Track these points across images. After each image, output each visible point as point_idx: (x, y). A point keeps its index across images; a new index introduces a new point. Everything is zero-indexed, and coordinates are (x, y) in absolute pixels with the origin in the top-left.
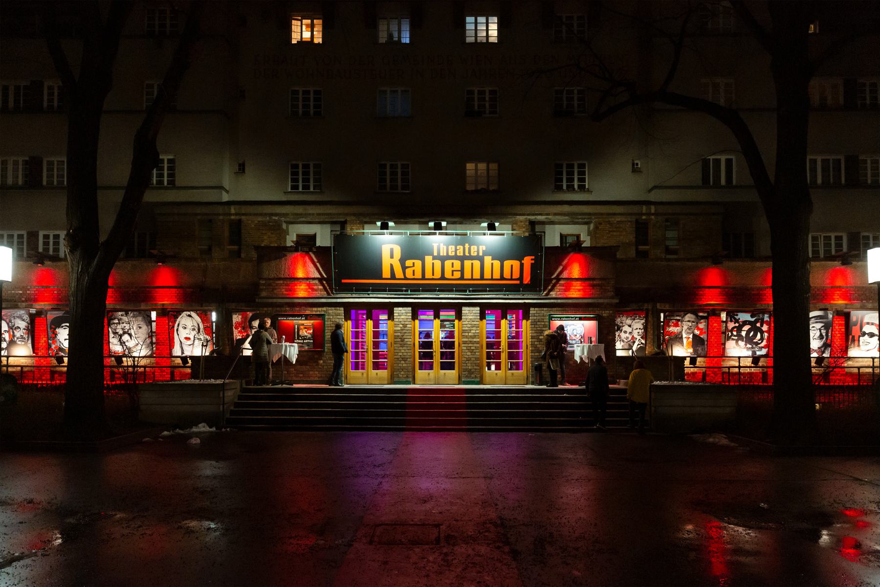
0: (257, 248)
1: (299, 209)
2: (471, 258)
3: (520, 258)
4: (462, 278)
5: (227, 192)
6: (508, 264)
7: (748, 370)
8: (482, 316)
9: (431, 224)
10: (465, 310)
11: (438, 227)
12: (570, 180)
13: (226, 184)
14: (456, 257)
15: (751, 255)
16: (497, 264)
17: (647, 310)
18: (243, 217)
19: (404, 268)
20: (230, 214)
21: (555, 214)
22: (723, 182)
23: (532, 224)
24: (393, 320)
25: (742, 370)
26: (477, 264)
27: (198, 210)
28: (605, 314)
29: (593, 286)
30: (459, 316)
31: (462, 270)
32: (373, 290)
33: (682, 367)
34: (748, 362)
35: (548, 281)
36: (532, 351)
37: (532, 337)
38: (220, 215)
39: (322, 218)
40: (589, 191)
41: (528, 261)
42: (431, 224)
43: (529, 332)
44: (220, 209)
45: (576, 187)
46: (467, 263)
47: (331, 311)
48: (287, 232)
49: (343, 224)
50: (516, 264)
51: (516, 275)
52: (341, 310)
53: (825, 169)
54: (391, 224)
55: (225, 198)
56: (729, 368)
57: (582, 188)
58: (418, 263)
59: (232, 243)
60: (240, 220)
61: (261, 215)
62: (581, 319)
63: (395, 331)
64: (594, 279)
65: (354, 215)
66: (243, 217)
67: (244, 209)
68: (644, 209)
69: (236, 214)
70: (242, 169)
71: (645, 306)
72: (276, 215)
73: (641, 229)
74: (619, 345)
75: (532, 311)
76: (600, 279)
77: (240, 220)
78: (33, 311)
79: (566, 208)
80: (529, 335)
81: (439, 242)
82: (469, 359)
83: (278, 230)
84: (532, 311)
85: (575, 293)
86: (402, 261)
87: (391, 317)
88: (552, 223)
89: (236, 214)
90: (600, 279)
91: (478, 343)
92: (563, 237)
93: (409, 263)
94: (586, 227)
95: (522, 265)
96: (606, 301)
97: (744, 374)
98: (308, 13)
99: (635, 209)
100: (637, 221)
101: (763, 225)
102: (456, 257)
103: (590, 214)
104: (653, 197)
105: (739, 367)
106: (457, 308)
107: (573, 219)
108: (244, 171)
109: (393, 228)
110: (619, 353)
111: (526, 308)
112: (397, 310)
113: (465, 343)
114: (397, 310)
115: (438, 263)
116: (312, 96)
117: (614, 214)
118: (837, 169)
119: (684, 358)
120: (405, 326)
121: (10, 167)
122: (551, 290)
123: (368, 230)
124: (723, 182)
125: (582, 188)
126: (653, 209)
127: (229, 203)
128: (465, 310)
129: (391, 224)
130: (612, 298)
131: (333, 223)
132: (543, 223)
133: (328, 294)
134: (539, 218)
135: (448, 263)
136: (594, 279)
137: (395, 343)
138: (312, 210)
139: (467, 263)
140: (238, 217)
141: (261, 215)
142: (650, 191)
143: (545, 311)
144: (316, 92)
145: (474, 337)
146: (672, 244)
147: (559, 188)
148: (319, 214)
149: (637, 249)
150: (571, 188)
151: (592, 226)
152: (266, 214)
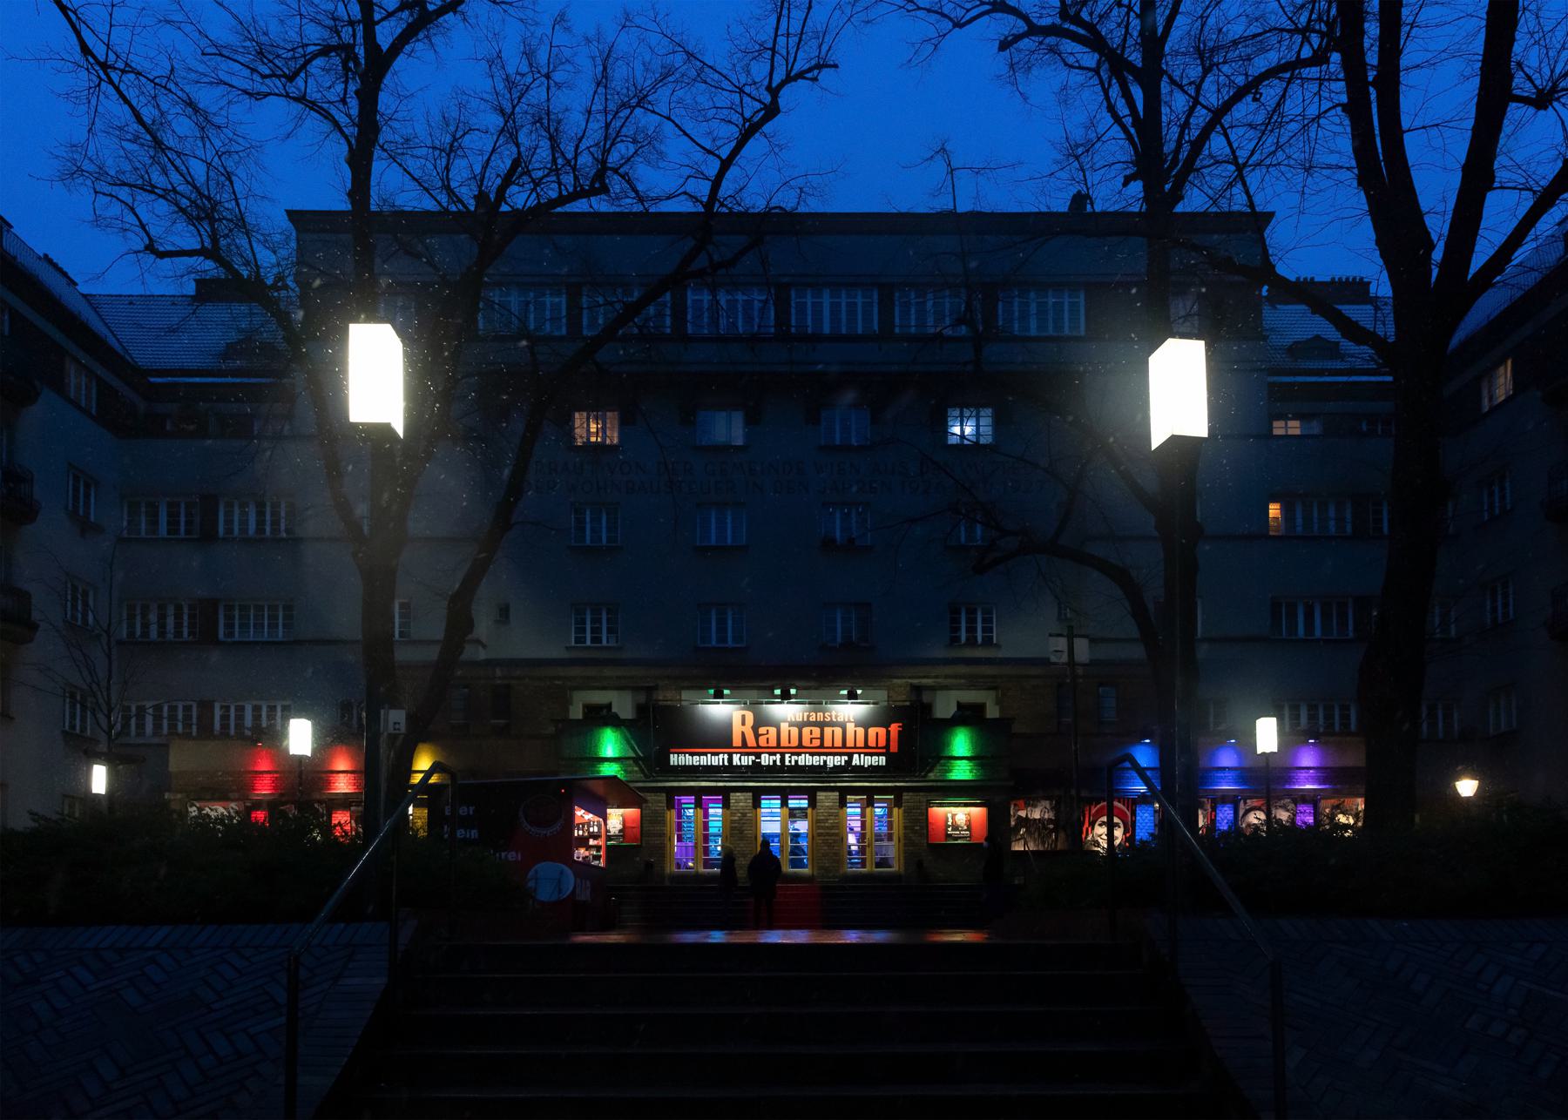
3: (886, 725)
4: (822, 746)
5: (484, 646)
6: (872, 731)
9: (778, 692)
12: (971, 630)
14: (815, 724)
16: (861, 731)
19: (757, 736)
21: (947, 677)
23: (917, 689)
26: (838, 731)
31: (822, 738)
37: (905, 828)
40: (998, 646)
42: (778, 692)
45: (980, 639)
46: (828, 731)
49: (650, 690)
50: (882, 731)
51: (882, 742)
52: (663, 797)
54: (726, 692)
57: (988, 642)
58: (773, 730)
62: (966, 805)
74: (556, 333)
75: (906, 796)
79: (962, 670)
81: (787, 712)
84: (906, 796)
85: (962, 772)
86: (755, 728)
93: (762, 730)
95: (888, 733)
98: (595, 408)
102: (815, 724)
103: (994, 677)
107: (973, 683)
108: (507, 617)
110: (564, 331)
112: (734, 796)
114: (734, 796)
115: (795, 731)
120: (744, 815)
123: (685, 695)
125: (988, 642)
127: (489, 663)
128: (821, 796)
129: (726, 692)
131: (635, 689)
132: (933, 689)
134: (925, 681)
135: (806, 730)
138: (608, 672)
139: (828, 731)
143: (922, 797)
150: (972, 642)
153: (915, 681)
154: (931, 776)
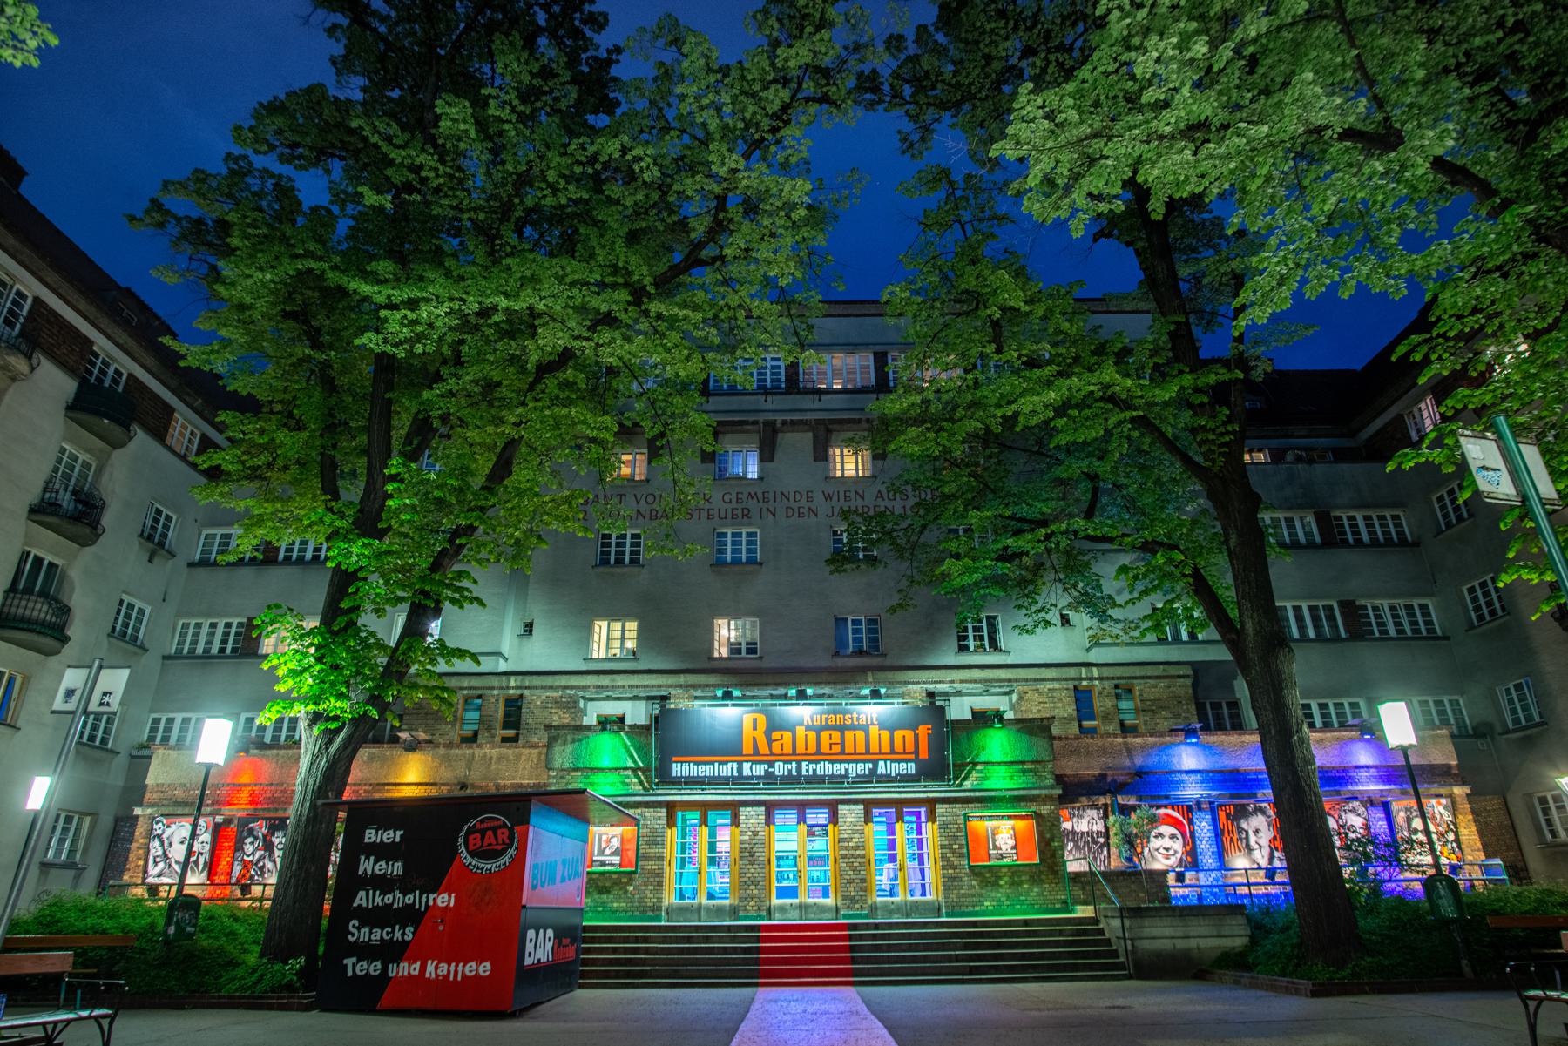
0: (548, 727)
1: (605, 680)
2: (853, 728)
4: (843, 752)
5: (506, 659)
6: (898, 734)
7: (1262, 890)
8: (868, 818)
10: (843, 810)
11: (801, 695)
13: (505, 650)
15: (1238, 726)
16: (886, 735)
17: (1106, 805)
18: (526, 692)
19: (770, 741)
20: (508, 688)
21: (962, 682)
22: (1392, 632)
23: (931, 695)
24: (737, 825)
25: (1254, 890)
26: (860, 735)
27: (465, 682)
28: (1045, 810)
29: (1024, 772)
30: (834, 818)
31: (842, 743)
32: (686, 783)
33: (1164, 886)
34: (1260, 877)
35: (960, 767)
36: (943, 868)
37: (942, 847)
38: (493, 688)
39: (636, 692)
41: (923, 731)
43: (937, 839)
44: (495, 682)
46: (849, 735)
47: (649, 813)
48: (584, 712)
50: (909, 734)
51: (910, 747)
52: (663, 813)
53: (1316, 619)
54: (737, 693)
55: (503, 666)
56: (1234, 885)
59: (506, 726)
60: (521, 696)
61: (551, 688)
62: (1010, 817)
63: (742, 842)
64: (1023, 763)
65: (680, 686)
66: (526, 692)
67: (528, 681)
68: (1084, 672)
69: (517, 688)
70: (529, 628)
71: (1102, 800)
72: (572, 688)
73: (1082, 698)
75: (940, 808)
76: (1032, 762)
77: (521, 696)
78: (219, 819)
79: (977, 674)
80: (938, 844)
81: (803, 713)
82: (850, 882)
83: (571, 705)
84: (940, 808)
86: (768, 733)
87: (735, 822)
88: (959, 693)
89: (517, 688)
90: (1032, 762)
91: (863, 856)
92: (389, 296)
93: (776, 735)
94: (1006, 698)
95: (916, 736)
96: (1044, 792)
97: (1257, 896)
99: (1072, 672)
100: (1075, 687)
101: (1242, 690)
104: (1096, 655)
105: (1249, 885)
106: (832, 807)
107: (987, 687)
109: (738, 698)
111: (931, 804)
112: (743, 812)
113: (843, 857)
114: (743, 812)
116: (628, 541)
117: (1044, 680)
118: (1331, 617)
119: (1164, 873)
120: (755, 833)
121: (205, 630)
122: (965, 779)
124: (1392, 632)
126: (1095, 672)
128: (843, 810)
130: (1052, 787)
131: (649, 698)
133: (645, 789)
136: (1023, 763)
137: (741, 858)
138: (621, 680)
139: (849, 735)
140: (518, 692)
141: (551, 688)
142: (1088, 650)
143: (959, 809)
144: (633, 536)
145: (857, 848)
146: (1130, 720)
147: (963, 648)
148: (631, 687)
149: (1080, 726)
151: (1014, 697)
152: (558, 688)
153: (931, 687)
154: (967, 784)
